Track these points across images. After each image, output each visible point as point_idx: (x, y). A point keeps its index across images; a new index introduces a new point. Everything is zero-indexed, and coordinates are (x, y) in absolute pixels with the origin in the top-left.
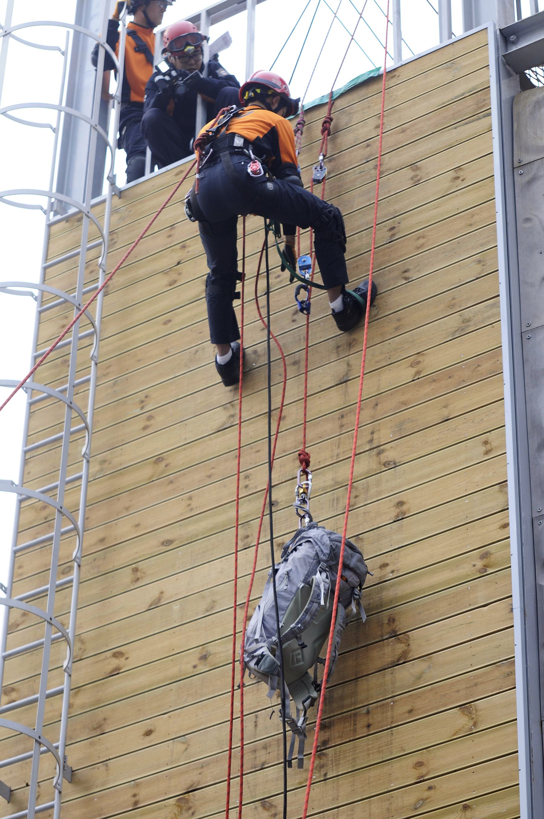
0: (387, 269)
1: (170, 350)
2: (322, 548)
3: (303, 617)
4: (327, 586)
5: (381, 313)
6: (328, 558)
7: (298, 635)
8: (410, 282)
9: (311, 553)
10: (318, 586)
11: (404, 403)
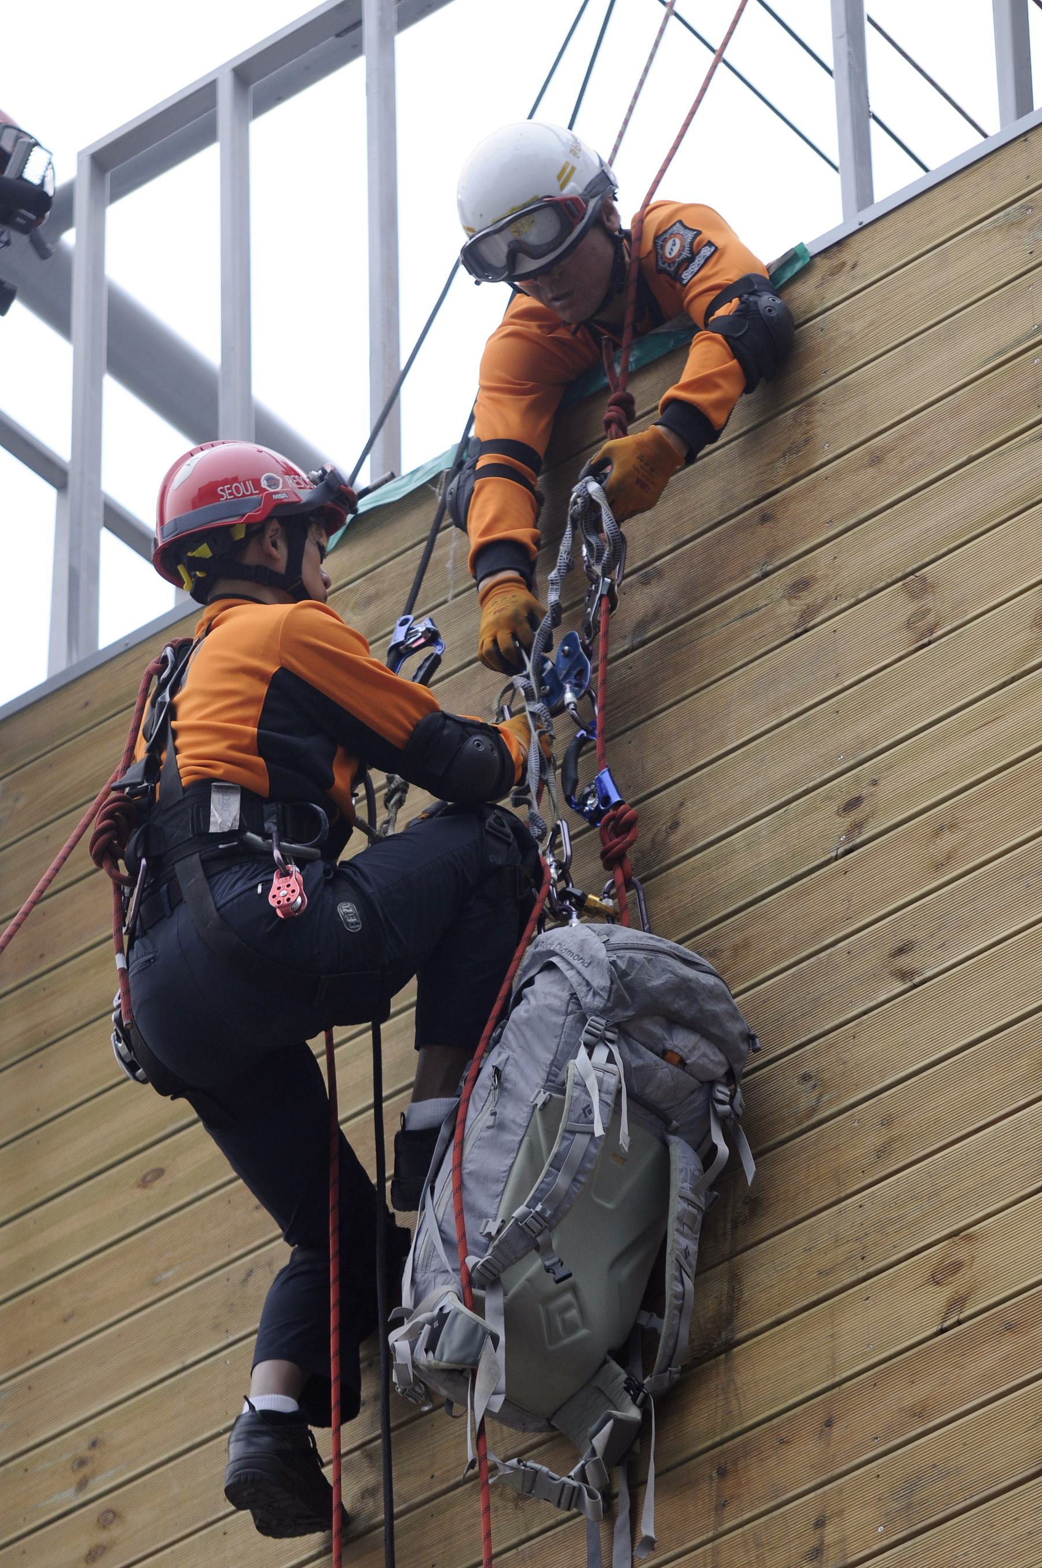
0: (840, 945)
2: (587, 973)
3: (547, 1180)
4: (611, 1081)
5: (830, 1102)
6: (608, 1000)
7: (539, 1239)
8: (916, 986)
9: (556, 996)
10: (581, 1085)
11: (919, 1412)
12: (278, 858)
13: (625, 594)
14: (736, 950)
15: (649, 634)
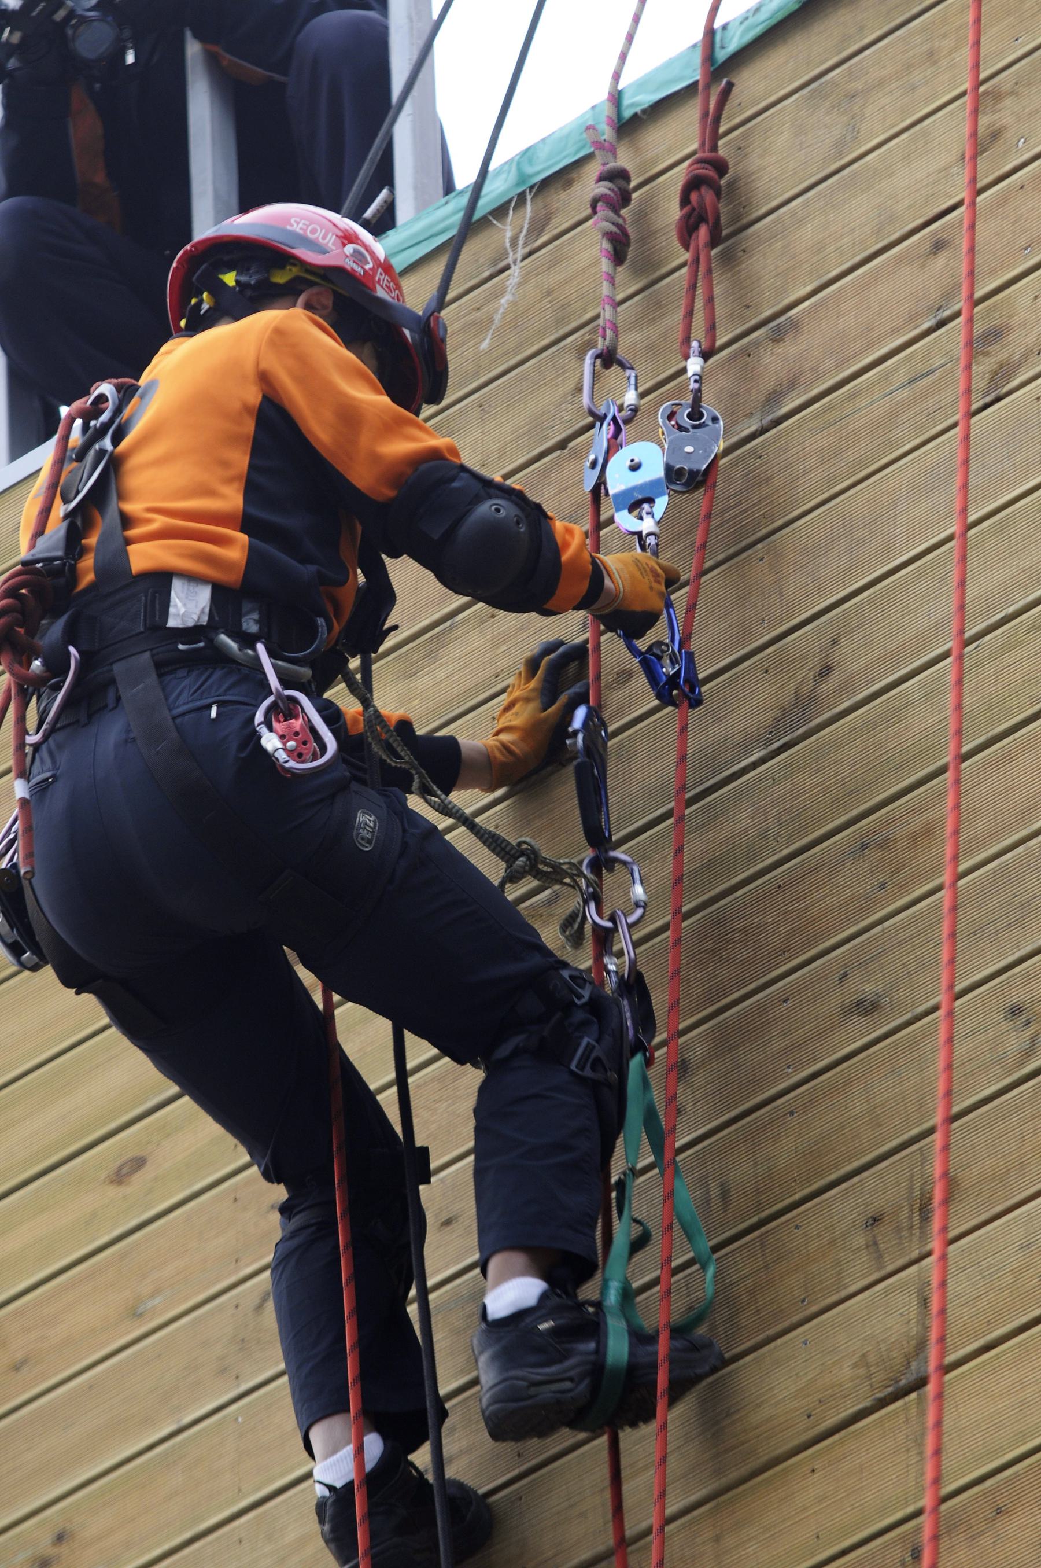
1: (150, 1304)
12: (277, 689)
13: (749, 355)
14: (914, 839)
15: (785, 410)
